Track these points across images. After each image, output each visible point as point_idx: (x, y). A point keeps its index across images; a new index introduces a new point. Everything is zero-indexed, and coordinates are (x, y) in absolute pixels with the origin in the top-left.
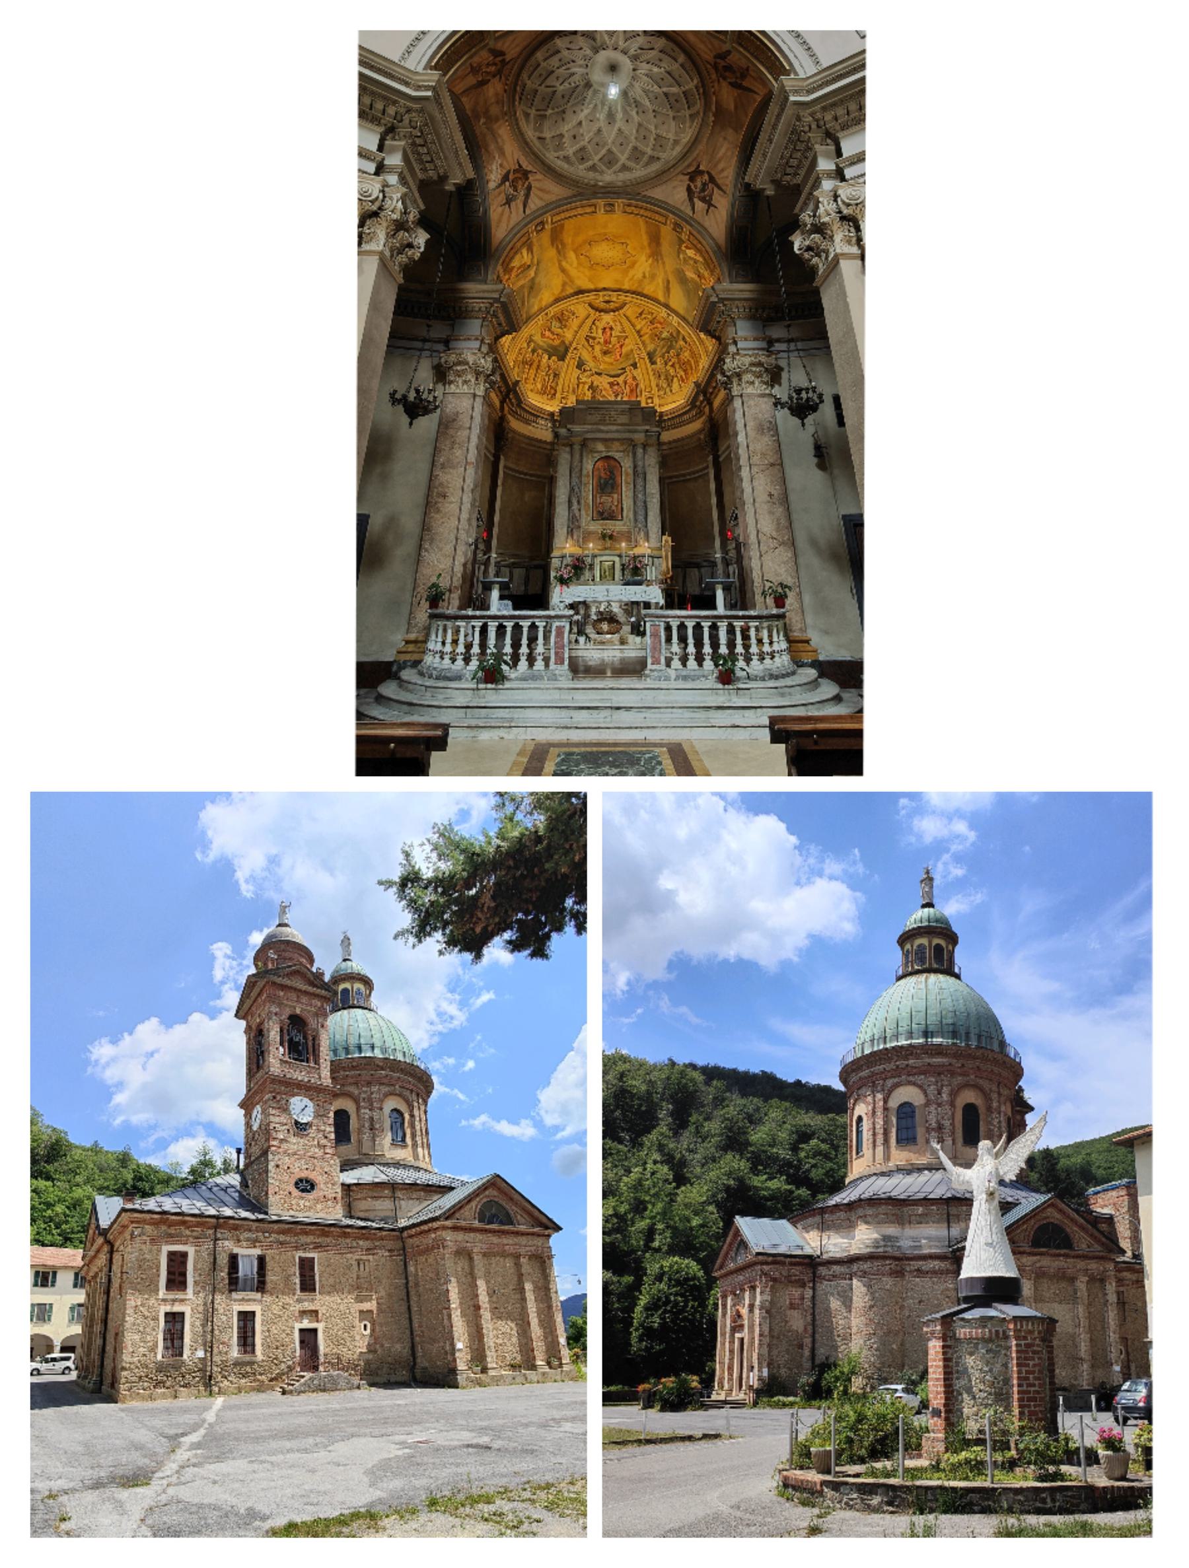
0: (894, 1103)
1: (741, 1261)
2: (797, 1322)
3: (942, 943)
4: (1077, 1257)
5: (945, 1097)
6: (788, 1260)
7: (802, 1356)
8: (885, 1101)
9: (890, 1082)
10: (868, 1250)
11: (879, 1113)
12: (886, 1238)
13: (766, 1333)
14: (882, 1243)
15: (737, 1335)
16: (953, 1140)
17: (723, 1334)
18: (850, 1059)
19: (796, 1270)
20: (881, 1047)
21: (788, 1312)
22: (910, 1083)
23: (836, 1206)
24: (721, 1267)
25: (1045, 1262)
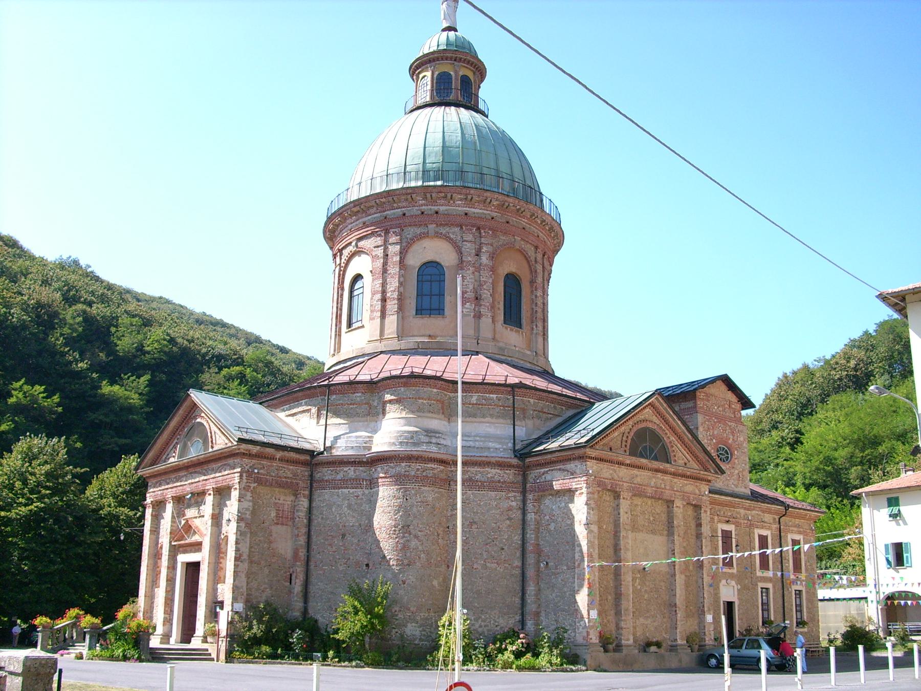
0: (416, 259)
1: (195, 452)
2: (285, 543)
3: (470, 74)
4: (674, 474)
5: (484, 259)
6: (279, 454)
7: (290, 592)
8: (403, 254)
9: (411, 232)
10: (350, 452)
11: (394, 270)
12: (429, 432)
13: (245, 556)
14: (424, 439)
15: (184, 558)
16: (493, 318)
17: (156, 555)
18: (335, 208)
19: (288, 471)
20: (400, 185)
21: (275, 529)
22: (438, 235)
23: (351, 383)
24: (154, 462)
25: (642, 476)
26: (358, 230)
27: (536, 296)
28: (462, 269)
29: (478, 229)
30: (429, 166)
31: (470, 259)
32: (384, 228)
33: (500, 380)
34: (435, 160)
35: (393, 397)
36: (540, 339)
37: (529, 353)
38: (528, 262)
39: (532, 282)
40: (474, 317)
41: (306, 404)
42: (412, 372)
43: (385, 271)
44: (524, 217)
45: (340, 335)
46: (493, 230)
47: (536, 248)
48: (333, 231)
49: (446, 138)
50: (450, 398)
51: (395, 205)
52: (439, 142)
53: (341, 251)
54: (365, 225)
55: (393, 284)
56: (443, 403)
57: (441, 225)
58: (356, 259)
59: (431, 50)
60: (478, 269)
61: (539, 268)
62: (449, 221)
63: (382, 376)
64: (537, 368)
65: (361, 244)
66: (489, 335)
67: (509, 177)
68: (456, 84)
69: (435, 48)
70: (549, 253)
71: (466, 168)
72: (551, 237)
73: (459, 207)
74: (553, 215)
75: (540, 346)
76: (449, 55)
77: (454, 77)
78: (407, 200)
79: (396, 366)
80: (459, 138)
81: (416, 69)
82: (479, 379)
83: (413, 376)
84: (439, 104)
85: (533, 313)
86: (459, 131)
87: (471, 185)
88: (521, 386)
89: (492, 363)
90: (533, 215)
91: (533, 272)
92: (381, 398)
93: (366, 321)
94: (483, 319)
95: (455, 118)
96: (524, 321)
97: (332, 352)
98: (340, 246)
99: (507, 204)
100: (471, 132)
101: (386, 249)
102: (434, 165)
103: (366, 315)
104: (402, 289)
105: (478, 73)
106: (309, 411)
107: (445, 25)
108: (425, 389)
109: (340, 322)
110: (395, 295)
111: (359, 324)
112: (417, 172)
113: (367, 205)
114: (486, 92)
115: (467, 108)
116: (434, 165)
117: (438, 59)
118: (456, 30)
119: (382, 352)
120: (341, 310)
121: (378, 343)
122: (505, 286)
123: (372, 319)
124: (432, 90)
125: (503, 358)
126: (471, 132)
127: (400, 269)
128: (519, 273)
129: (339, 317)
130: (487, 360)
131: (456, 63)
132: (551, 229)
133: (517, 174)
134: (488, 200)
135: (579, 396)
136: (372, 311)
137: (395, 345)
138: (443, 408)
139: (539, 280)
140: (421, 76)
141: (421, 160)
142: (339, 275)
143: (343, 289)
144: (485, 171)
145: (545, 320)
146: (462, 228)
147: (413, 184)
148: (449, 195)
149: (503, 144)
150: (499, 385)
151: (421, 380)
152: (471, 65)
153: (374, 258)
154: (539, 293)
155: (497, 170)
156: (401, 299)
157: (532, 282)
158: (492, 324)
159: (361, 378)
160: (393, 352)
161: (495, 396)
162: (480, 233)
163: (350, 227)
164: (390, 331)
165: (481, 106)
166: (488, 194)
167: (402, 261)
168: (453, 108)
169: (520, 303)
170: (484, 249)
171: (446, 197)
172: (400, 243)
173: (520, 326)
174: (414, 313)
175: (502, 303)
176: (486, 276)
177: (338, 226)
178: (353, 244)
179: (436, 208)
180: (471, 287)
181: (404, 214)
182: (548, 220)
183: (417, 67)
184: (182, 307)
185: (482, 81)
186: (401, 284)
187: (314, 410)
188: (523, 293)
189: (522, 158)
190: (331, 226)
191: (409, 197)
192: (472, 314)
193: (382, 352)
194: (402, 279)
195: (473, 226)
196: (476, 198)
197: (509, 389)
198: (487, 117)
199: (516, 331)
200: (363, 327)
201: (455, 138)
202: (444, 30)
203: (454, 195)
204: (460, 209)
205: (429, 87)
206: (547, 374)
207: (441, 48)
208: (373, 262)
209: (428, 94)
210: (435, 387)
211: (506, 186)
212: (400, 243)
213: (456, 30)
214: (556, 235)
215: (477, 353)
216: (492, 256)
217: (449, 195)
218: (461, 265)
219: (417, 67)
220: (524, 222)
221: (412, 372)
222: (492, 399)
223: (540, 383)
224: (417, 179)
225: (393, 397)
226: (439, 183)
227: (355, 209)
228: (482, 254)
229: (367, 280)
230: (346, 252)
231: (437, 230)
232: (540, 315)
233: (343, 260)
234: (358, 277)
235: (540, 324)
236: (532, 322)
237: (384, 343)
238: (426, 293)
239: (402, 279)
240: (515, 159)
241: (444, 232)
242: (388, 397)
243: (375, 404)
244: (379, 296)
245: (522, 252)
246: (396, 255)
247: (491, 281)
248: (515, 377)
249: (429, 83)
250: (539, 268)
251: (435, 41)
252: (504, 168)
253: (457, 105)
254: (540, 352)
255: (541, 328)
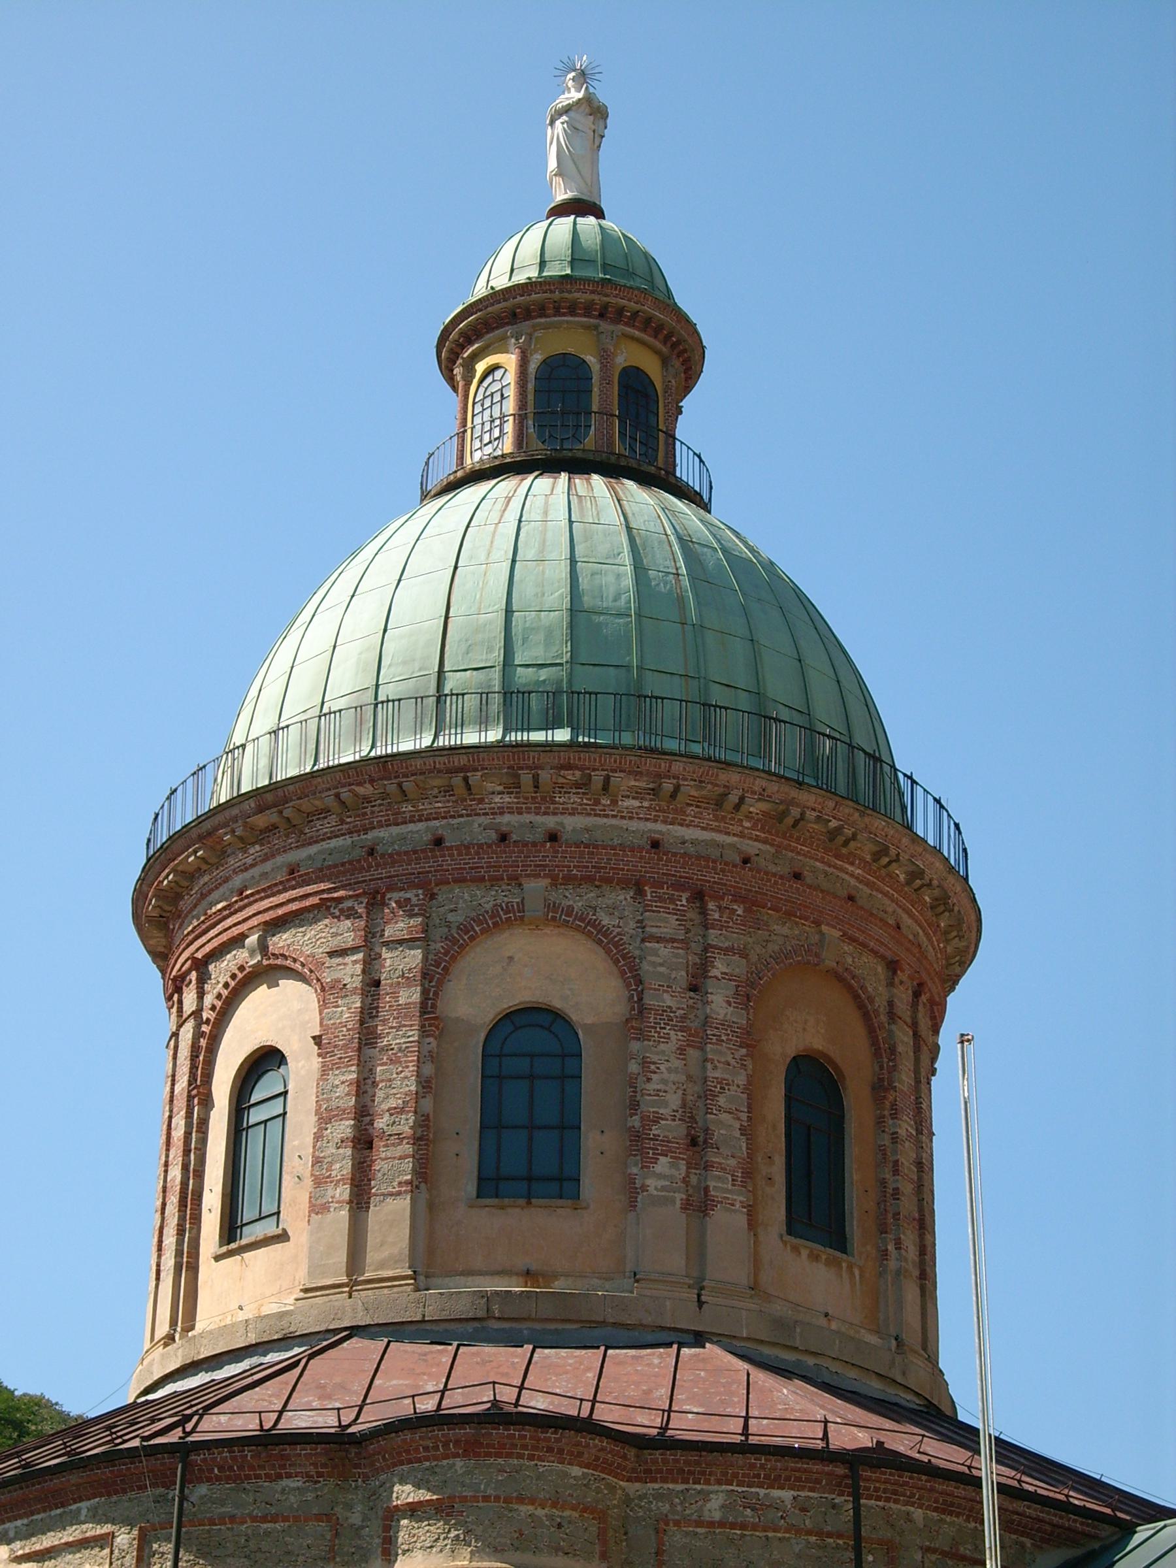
0: (476, 1000)
3: (651, 366)
8: (433, 978)
9: (462, 902)
11: (399, 1035)
18: (185, 814)
22: (557, 917)
26: (269, 892)
27: (895, 1138)
28: (641, 1036)
29: (699, 896)
30: (524, 676)
31: (668, 1001)
32: (364, 886)
33: (806, 1435)
34: (543, 651)
35: (424, 1495)
36: (911, 1293)
37: (873, 1339)
38: (866, 1016)
39: (881, 1087)
40: (686, 1206)
41: (96, 1517)
42: (495, 1403)
43: (367, 1036)
44: (850, 859)
45: (194, 1268)
46: (752, 903)
47: (893, 966)
48: (172, 896)
49: (584, 583)
50: (627, 1500)
51: (407, 808)
52: (558, 596)
53: (201, 966)
54: (295, 876)
55: (397, 1086)
56: (601, 1516)
57: (568, 879)
58: (260, 998)
59: (520, 278)
60: (698, 1035)
61: (903, 1038)
62: (594, 867)
63: (372, 1418)
64: (906, 1398)
65: (280, 941)
66: (740, 1275)
67: (798, 719)
68: (603, 395)
69: (533, 273)
70: (934, 987)
71: (654, 685)
72: (938, 923)
73: (630, 820)
74: (949, 851)
75: (912, 1316)
76: (582, 297)
77: (597, 372)
78: (448, 790)
79: (413, 1380)
80: (628, 581)
81: (461, 344)
82: (646, 1422)
83: (498, 1417)
84: (548, 466)
85: (887, 1195)
86: (626, 557)
87: (671, 745)
88: (879, 1458)
89: (761, 1378)
90: (884, 851)
91: (882, 1051)
92: (377, 1496)
93: (295, 1217)
94: (718, 1215)
95: (612, 515)
96: (857, 1227)
97: (163, 1329)
98: (202, 947)
99: (795, 812)
100: (668, 560)
101: (371, 963)
102: (544, 674)
103: (296, 1196)
104: (427, 1104)
105: (676, 363)
106: (104, 1541)
107: (561, 194)
108: (544, 1466)
109: (197, 1219)
110: (406, 1124)
111: (267, 1228)
112: (484, 695)
113: (306, 805)
114: (701, 425)
115: (646, 480)
116: (544, 674)
117: (542, 310)
118: (599, 214)
119: (354, 1331)
120: (200, 1175)
121: (340, 1299)
122: (789, 1099)
123: (318, 1208)
124: (520, 419)
125: (790, 1356)
126: (668, 560)
127: (424, 1032)
128: (834, 1052)
129: (190, 1201)
130: (746, 1366)
131: (604, 326)
132: (942, 902)
133: (826, 712)
134: (733, 798)
135: (1077, 1499)
136: (318, 1182)
137: (402, 1304)
138: (602, 1535)
139: (905, 1079)
140: (480, 367)
141: (497, 656)
142: (195, 1049)
143: (207, 1102)
144: (718, 695)
145: (924, 1224)
146: (640, 892)
147: (471, 737)
148: (597, 779)
149: (761, 604)
150: (805, 1454)
151: (528, 1432)
152: (656, 332)
153: (328, 992)
154: (905, 1127)
155: (758, 694)
156: (424, 1139)
157: (881, 1087)
158: (747, 1232)
159: (297, 1421)
160: (396, 1331)
161: (786, 1495)
162: (703, 912)
163: (237, 881)
164: (385, 1253)
165: (686, 470)
166: (734, 777)
167: (428, 1008)
168: (596, 479)
169: (843, 1165)
170: (719, 967)
171: (719, 801)
172: (422, 940)
173: (838, 1240)
174: (472, 1188)
175: (780, 1161)
176: (725, 1065)
177: (191, 876)
178: (252, 940)
179: (550, 822)
180: (674, 1100)
181: (438, 842)
182: (935, 871)
183: (468, 338)
184: (502, 1208)
185: (687, 389)
186: (425, 1085)
187: (124, 1538)
188: (852, 1128)
189: (839, 660)
190: (167, 879)
191: (457, 780)
192: (679, 1197)
193: (354, 1331)
194: (428, 1070)
195: (679, 886)
196: (689, 789)
197: (841, 1470)
198: (707, 508)
199: (829, 1263)
200: (283, 1237)
201: (616, 580)
202: (559, 211)
203: (617, 779)
204: (634, 825)
205: (510, 406)
206: (938, 1416)
207: (552, 271)
208: (323, 1005)
209: (509, 427)
210: (576, 1458)
211: (788, 748)
212: (422, 940)
213: (599, 214)
214: (958, 924)
215: (699, 1339)
216: (747, 994)
217: (597, 779)
218: (638, 1018)
219: (468, 338)
220: (851, 876)
221: (495, 1403)
222: (776, 1506)
223: (905, 1440)
224: (484, 722)
225: (424, 1495)
226: (562, 735)
227: (261, 821)
228: (710, 985)
229: (302, 1067)
230: (222, 972)
231: (554, 896)
232: (907, 1205)
233: (209, 1000)
234: (265, 1060)
235: (909, 1240)
236: (883, 1230)
237: (364, 1295)
238: (511, 1122)
239: (428, 1070)
240: (816, 659)
241: (578, 905)
242: (405, 1493)
243: (356, 1519)
244: (344, 1128)
245: (842, 979)
246: (409, 982)
247: (741, 1079)
248: (854, 1430)
249: (511, 392)
250: (903, 1038)
251: (521, 254)
252: (781, 689)
253: (613, 470)
254: (912, 1339)
255: (912, 1253)
